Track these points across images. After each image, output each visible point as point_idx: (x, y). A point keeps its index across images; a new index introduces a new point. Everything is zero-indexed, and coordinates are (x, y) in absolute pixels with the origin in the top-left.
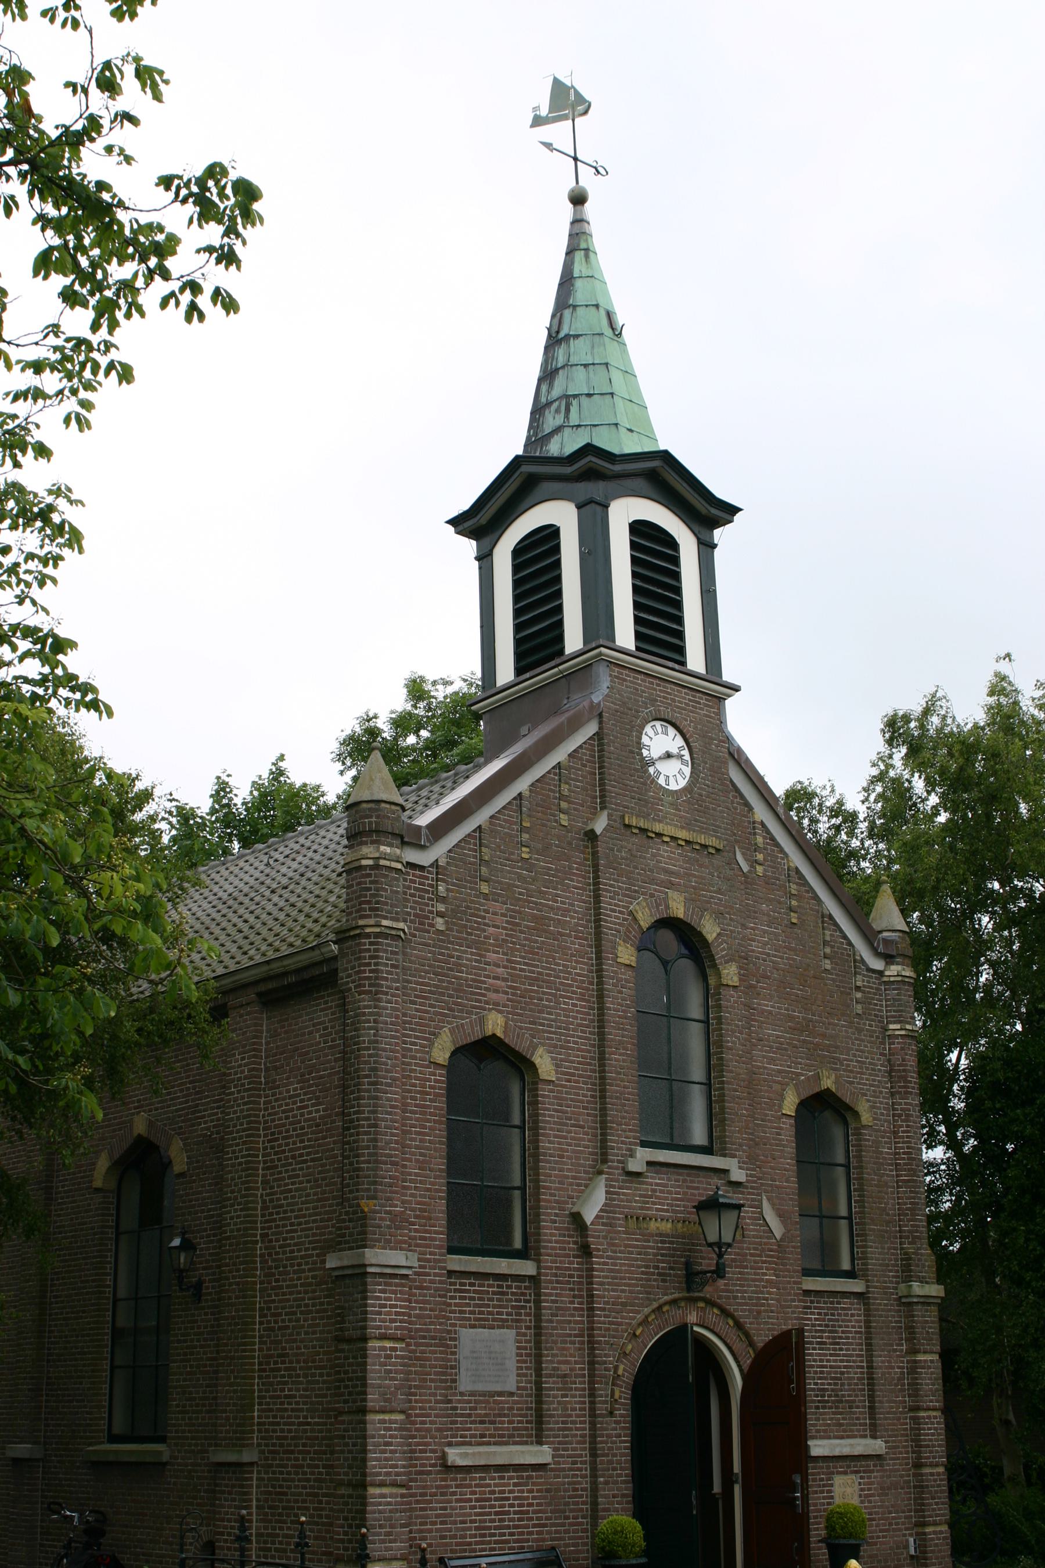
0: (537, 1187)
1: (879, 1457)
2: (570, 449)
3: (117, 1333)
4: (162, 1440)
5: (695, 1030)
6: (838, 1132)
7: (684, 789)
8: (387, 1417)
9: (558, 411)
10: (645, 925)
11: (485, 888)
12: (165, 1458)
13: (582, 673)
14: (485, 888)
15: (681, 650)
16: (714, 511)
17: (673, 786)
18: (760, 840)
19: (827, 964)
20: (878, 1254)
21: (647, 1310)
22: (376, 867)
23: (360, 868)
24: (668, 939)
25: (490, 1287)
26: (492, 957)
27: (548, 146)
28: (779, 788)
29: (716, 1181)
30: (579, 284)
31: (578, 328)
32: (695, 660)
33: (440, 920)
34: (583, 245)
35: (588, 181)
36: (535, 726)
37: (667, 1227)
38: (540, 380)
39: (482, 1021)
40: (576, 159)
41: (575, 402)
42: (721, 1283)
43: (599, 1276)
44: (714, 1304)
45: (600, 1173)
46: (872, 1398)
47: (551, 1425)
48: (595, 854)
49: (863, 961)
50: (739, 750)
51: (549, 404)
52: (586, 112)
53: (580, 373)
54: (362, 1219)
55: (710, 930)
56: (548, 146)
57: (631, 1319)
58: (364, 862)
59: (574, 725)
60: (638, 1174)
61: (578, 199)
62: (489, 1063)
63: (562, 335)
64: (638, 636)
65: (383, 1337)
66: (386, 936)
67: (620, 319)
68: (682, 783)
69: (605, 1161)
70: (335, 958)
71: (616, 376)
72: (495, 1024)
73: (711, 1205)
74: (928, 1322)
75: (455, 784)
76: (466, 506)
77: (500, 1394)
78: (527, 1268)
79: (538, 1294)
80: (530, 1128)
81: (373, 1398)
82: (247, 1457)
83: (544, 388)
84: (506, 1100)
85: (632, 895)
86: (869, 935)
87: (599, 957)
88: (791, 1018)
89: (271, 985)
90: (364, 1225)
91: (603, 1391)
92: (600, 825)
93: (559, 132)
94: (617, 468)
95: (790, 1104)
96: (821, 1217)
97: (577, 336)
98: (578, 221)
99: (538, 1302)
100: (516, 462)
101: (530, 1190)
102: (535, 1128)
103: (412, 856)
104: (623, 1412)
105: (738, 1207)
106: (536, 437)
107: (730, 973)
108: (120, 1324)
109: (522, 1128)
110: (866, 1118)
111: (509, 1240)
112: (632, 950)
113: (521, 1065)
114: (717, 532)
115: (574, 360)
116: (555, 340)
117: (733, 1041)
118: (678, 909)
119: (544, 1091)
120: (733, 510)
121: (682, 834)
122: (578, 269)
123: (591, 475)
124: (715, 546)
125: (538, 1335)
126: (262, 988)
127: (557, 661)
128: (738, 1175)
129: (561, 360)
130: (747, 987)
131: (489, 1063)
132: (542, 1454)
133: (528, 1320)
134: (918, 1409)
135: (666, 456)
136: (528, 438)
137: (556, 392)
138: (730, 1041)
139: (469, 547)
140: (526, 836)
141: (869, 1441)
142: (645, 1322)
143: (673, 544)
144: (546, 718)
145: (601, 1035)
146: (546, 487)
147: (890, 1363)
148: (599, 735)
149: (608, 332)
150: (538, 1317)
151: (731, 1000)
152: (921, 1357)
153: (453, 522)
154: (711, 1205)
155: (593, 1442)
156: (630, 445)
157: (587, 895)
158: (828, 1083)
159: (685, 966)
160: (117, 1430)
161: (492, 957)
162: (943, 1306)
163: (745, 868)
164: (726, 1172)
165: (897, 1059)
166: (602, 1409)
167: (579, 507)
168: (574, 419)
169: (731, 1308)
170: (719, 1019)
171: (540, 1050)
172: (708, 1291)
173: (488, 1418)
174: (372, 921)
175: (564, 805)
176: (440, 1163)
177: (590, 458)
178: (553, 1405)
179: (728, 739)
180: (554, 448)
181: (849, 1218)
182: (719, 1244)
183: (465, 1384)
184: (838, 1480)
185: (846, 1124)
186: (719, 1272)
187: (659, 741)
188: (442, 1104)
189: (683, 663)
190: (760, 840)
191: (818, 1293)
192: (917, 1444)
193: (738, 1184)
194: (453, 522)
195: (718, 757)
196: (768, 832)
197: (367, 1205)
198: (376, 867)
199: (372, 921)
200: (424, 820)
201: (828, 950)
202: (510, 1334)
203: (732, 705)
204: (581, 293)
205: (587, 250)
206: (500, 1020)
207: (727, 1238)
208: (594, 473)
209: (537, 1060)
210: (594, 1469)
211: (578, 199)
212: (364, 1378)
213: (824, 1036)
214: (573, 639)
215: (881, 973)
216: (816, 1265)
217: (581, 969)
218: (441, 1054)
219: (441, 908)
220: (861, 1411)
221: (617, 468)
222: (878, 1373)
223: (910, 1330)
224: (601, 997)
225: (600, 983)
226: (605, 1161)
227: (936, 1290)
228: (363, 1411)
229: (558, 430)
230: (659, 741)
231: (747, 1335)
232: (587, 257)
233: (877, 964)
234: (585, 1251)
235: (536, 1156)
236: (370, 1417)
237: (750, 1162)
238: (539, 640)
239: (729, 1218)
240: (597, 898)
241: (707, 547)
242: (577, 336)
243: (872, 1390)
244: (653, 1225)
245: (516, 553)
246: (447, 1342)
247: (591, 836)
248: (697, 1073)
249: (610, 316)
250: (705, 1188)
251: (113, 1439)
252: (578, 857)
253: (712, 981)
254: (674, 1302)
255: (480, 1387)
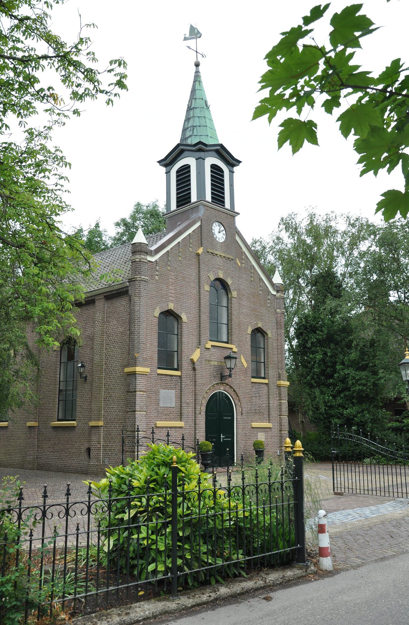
0: (182, 351)
1: (270, 428)
2: (194, 142)
3: (60, 391)
4: (74, 420)
5: (225, 309)
6: (261, 339)
7: (223, 242)
8: (141, 413)
9: (190, 130)
10: (212, 280)
11: (169, 268)
12: (75, 425)
13: (196, 208)
14: (169, 268)
15: (223, 202)
16: (234, 162)
17: (221, 241)
18: (243, 257)
19: (261, 292)
20: (272, 373)
21: (210, 386)
22: (140, 261)
23: (135, 261)
24: (218, 283)
25: (168, 378)
26: (170, 287)
27: (189, 47)
28: (249, 242)
29: (229, 351)
30: (197, 91)
31: (197, 105)
32: (227, 205)
33: (157, 277)
34: (198, 80)
35: (200, 59)
36: (182, 223)
37: (216, 363)
38: (185, 121)
39: (168, 305)
40: (197, 52)
41: (195, 128)
42: (230, 379)
43: (198, 376)
44: (228, 385)
45: (198, 348)
46: (269, 412)
47: (184, 416)
48: (199, 259)
49: (270, 292)
50: (239, 231)
51: (188, 128)
52: (200, 37)
53: (197, 119)
54: (135, 359)
55: (229, 282)
56: (189, 47)
57: (208, 388)
58: (137, 260)
59: (194, 223)
60: (209, 349)
61: (197, 65)
62: (170, 316)
63: (192, 107)
64: (212, 198)
65: (140, 391)
66: (143, 281)
67: (209, 103)
68: (223, 240)
69: (200, 345)
70: (128, 287)
71: (207, 121)
72: (171, 306)
73: (228, 358)
74: (285, 393)
75: (161, 239)
76: (163, 158)
77: (171, 407)
78: (178, 373)
79: (181, 381)
80: (179, 335)
81: (138, 408)
82: (101, 423)
83: (186, 123)
84: (173, 327)
85: (209, 271)
86: (272, 284)
87: (199, 288)
88: (250, 307)
89: (108, 294)
90: (136, 360)
91: (198, 407)
92: (200, 251)
93: (192, 43)
94: (208, 148)
95: (249, 331)
96: (257, 362)
97: (196, 108)
98: (197, 72)
99: (181, 383)
100: (178, 145)
101: (179, 352)
102: (181, 335)
103: (149, 258)
104: (203, 413)
105: (236, 358)
106: (184, 138)
107: (234, 294)
108: (61, 388)
109: (178, 335)
110: (270, 335)
111: (173, 366)
112: (209, 287)
113: (178, 318)
114: (234, 168)
115: (195, 115)
116: (190, 109)
117: (235, 312)
118: (221, 276)
119: (184, 325)
120: (239, 162)
121: (223, 255)
122: (197, 87)
123: (200, 150)
124: (233, 172)
125: (181, 392)
126: (106, 294)
127: (189, 204)
128: (235, 350)
129: (192, 115)
130: (239, 298)
131: (170, 316)
132: (181, 424)
133: (179, 388)
134: (281, 415)
135: (222, 146)
136: (181, 138)
137: (190, 125)
138: (234, 312)
139: (164, 169)
140: (180, 254)
141: (268, 423)
142: (210, 389)
143: (222, 171)
144: (186, 221)
145: (200, 310)
146: (186, 153)
147: (274, 403)
148: (201, 226)
149: (205, 107)
150: (181, 387)
151: (234, 301)
152: (282, 401)
153: (159, 162)
154: (228, 358)
155: (195, 421)
156: (210, 142)
157: (197, 270)
158: (260, 325)
159: (223, 291)
160: (60, 417)
161: (170, 287)
162: (289, 388)
163: (239, 264)
164: (232, 349)
165: (279, 319)
166: (198, 412)
167: (196, 159)
168: (195, 133)
169: (232, 386)
170: (231, 306)
171: (183, 314)
172: (227, 381)
173: (166, 414)
174: (139, 277)
175: (191, 245)
176: (156, 344)
177: (200, 145)
178: (184, 411)
179: (236, 228)
180: (189, 142)
181: (264, 363)
182: (230, 368)
183: (161, 405)
184: (259, 434)
185: (264, 337)
186: (230, 376)
187: (216, 228)
188: (157, 327)
189: (224, 206)
190: (243, 257)
191: (255, 383)
192: (281, 425)
193: (235, 352)
194: (159, 162)
195: (232, 232)
196: (246, 255)
197: (136, 355)
198: (140, 261)
199: (139, 277)
200: (153, 248)
201: (261, 288)
202: (174, 391)
203: (237, 218)
204: (198, 94)
205: (200, 81)
206: (173, 305)
207: (233, 367)
208: (201, 149)
209: (182, 316)
210: (195, 428)
211: (197, 65)
212: (135, 402)
213: (259, 312)
214: (194, 198)
215: (275, 295)
216: (255, 375)
217: (195, 291)
218: (157, 314)
219: (157, 273)
220: (266, 416)
221: (208, 148)
222: (271, 405)
223: (280, 394)
224: (200, 299)
225: (200, 295)
226: (200, 345)
227: (288, 383)
228: (135, 411)
229: (190, 136)
230: (216, 228)
231: (236, 393)
232: (200, 83)
233: (274, 293)
234: (194, 369)
235: (181, 343)
236: (136, 413)
237: (238, 346)
238: (185, 197)
239: (233, 361)
240: (199, 271)
241: (232, 172)
242: (196, 108)
243: (269, 410)
244: (212, 362)
245: (178, 172)
246: (157, 393)
247: (198, 255)
248: (225, 321)
249: (206, 102)
250: (227, 353)
251: (59, 420)
252: (194, 260)
253: (230, 296)
254: (217, 384)
255: (165, 406)
